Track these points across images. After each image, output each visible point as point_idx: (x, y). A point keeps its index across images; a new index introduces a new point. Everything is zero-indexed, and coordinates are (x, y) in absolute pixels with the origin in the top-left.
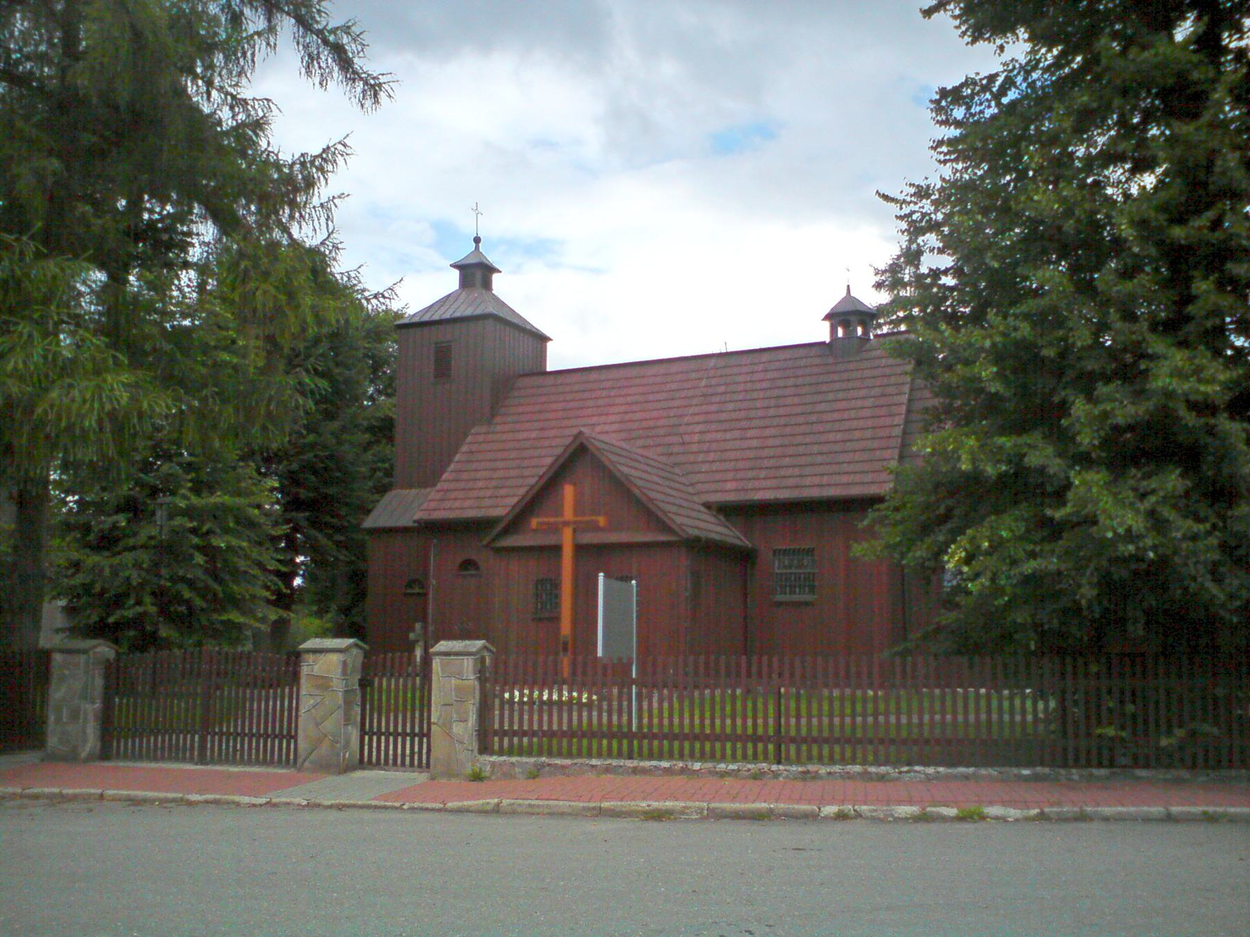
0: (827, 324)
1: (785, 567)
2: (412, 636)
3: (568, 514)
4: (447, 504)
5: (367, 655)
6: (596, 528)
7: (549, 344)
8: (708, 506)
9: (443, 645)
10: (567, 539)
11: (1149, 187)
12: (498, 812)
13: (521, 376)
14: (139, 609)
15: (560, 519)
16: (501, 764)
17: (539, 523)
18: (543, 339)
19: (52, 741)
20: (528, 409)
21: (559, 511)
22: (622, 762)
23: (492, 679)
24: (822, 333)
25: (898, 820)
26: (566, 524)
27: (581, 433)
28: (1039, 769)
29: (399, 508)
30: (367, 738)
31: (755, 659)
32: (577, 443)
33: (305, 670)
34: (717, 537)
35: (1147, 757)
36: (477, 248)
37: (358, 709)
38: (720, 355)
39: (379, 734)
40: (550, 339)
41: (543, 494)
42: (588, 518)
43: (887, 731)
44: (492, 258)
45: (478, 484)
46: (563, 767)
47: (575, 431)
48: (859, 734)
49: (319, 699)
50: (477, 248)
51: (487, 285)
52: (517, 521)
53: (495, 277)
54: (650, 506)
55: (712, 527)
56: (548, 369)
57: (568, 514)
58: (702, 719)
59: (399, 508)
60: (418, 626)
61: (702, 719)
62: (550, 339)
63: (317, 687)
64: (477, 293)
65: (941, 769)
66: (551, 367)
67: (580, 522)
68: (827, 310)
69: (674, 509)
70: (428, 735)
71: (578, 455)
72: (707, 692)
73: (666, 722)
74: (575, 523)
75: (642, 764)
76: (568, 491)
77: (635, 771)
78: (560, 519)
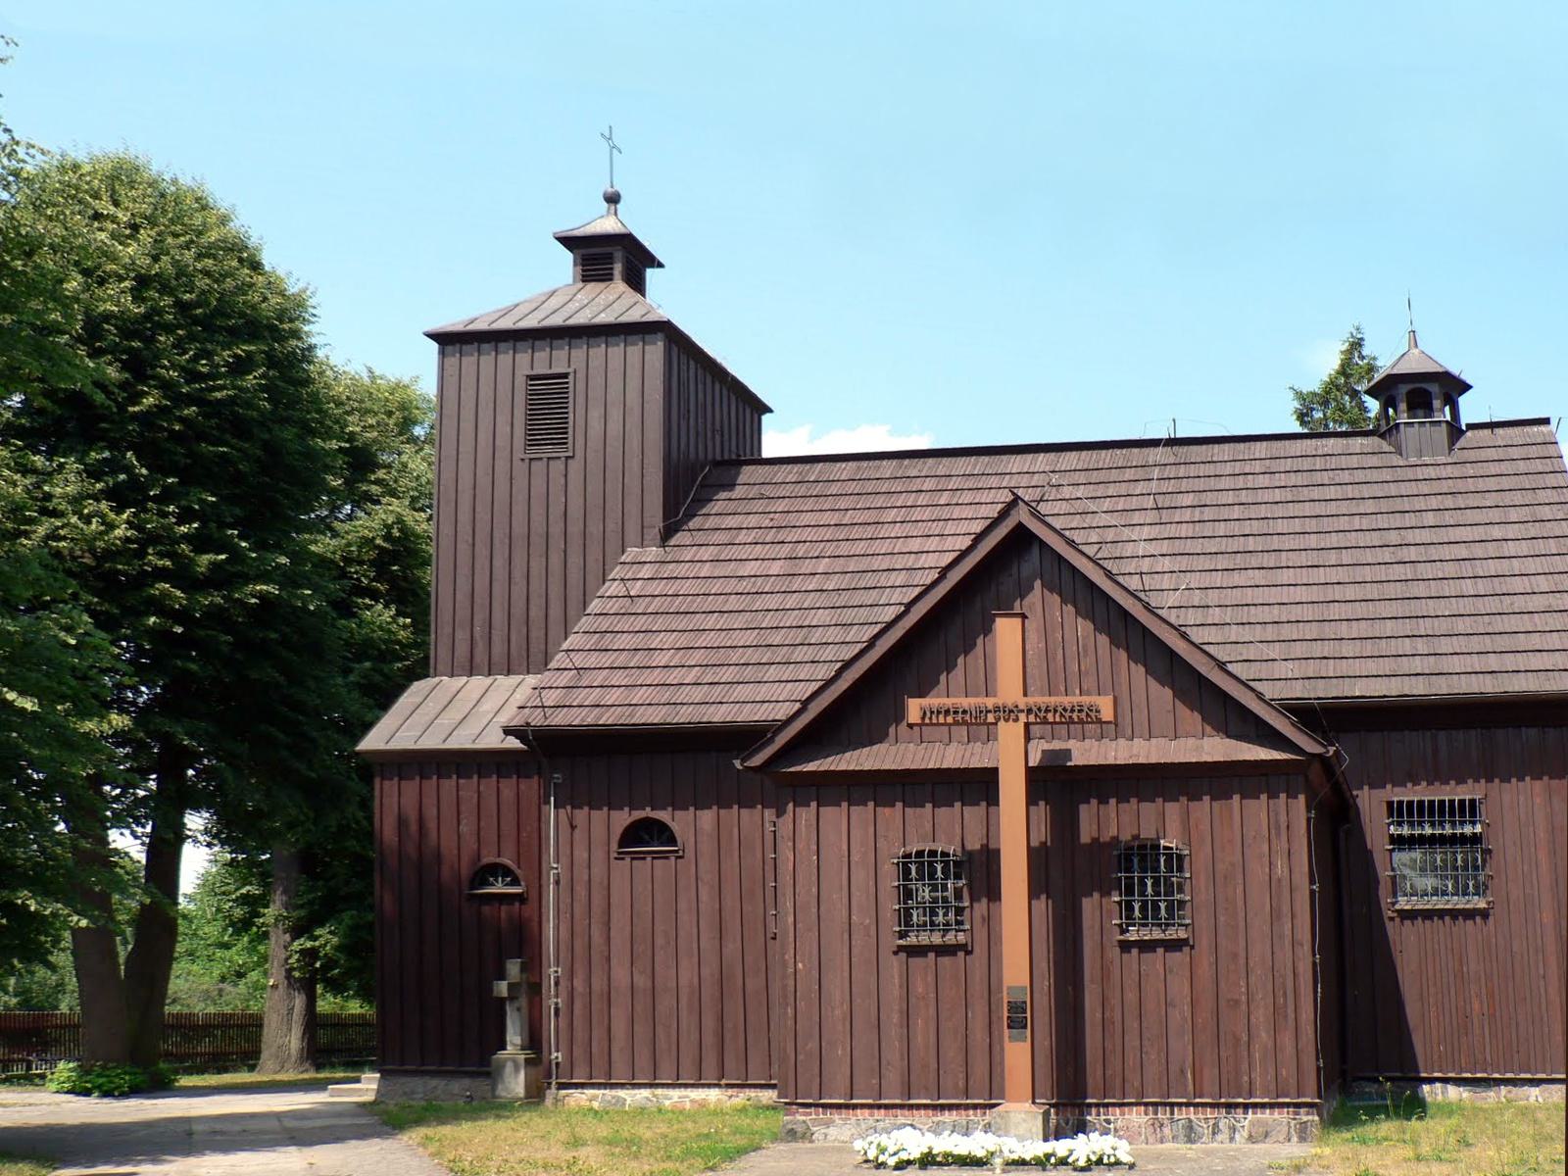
2: (502, 988)
3: (1009, 689)
4: (578, 697)
7: (766, 418)
10: (1010, 756)
11: (154, 788)
14: (1013, 788)
20: (730, 521)
26: (1009, 713)
29: (457, 710)
40: (769, 410)
42: (1075, 699)
45: (701, 636)
52: (867, 698)
56: (767, 452)
57: (1009, 689)
59: (457, 710)
60: (513, 968)
62: (769, 410)
65: (123, 967)
66: (767, 452)
78: (990, 702)
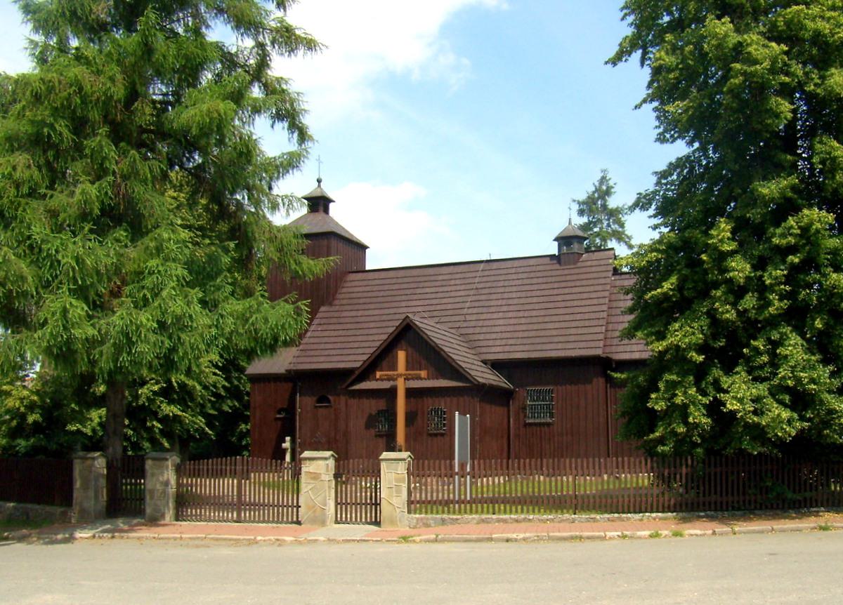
0: (556, 243)
1: (534, 401)
5: (337, 460)
6: (419, 378)
8: (485, 362)
9: (307, 454)
12: (436, 541)
13: (350, 272)
15: (395, 373)
16: (422, 519)
17: (380, 376)
18: (363, 248)
19: (148, 510)
21: (394, 367)
22: (489, 516)
23: (416, 472)
24: (553, 249)
25: (640, 538)
26: (401, 375)
27: (407, 317)
28: (708, 512)
30: (339, 506)
31: (591, 460)
32: (405, 323)
33: (304, 469)
34: (494, 383)
35: (800, 501)
36: (319, 186)
37: (333, 491)
38: (488, 261)
39: (288, 506)
40: (367, 247)
41: (383, 357)
43: (432, 508)
44: (330, 194)
46: (457, 519)
47: (403, 316)
48: (429, 507)
49: (313, 485)
50: (319, 186)
51: (326, 211)
52: (368, 370)
53: (331, 205)
54: (453, 364)
55: (491, 377)
56: (367, 268)
58: (288, 500)
60: (288, 439)
61: (288, 500)
62: (367, 247)
63: (312, 478)
64: (320, 216)
67: (410, 375)
68: (556, 234)
69: (469, 366)
70: (380, 504)
71: (406, 334)
72: (266, 474)
73: (536, 490)
74: (405, 375)
75: (501, 517)
76: (401, 355)
77: (499, 521)
